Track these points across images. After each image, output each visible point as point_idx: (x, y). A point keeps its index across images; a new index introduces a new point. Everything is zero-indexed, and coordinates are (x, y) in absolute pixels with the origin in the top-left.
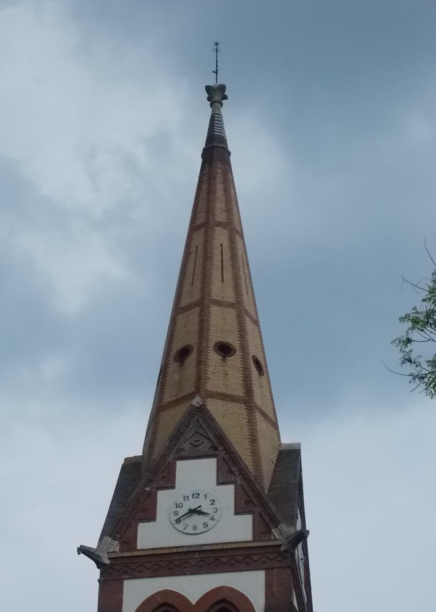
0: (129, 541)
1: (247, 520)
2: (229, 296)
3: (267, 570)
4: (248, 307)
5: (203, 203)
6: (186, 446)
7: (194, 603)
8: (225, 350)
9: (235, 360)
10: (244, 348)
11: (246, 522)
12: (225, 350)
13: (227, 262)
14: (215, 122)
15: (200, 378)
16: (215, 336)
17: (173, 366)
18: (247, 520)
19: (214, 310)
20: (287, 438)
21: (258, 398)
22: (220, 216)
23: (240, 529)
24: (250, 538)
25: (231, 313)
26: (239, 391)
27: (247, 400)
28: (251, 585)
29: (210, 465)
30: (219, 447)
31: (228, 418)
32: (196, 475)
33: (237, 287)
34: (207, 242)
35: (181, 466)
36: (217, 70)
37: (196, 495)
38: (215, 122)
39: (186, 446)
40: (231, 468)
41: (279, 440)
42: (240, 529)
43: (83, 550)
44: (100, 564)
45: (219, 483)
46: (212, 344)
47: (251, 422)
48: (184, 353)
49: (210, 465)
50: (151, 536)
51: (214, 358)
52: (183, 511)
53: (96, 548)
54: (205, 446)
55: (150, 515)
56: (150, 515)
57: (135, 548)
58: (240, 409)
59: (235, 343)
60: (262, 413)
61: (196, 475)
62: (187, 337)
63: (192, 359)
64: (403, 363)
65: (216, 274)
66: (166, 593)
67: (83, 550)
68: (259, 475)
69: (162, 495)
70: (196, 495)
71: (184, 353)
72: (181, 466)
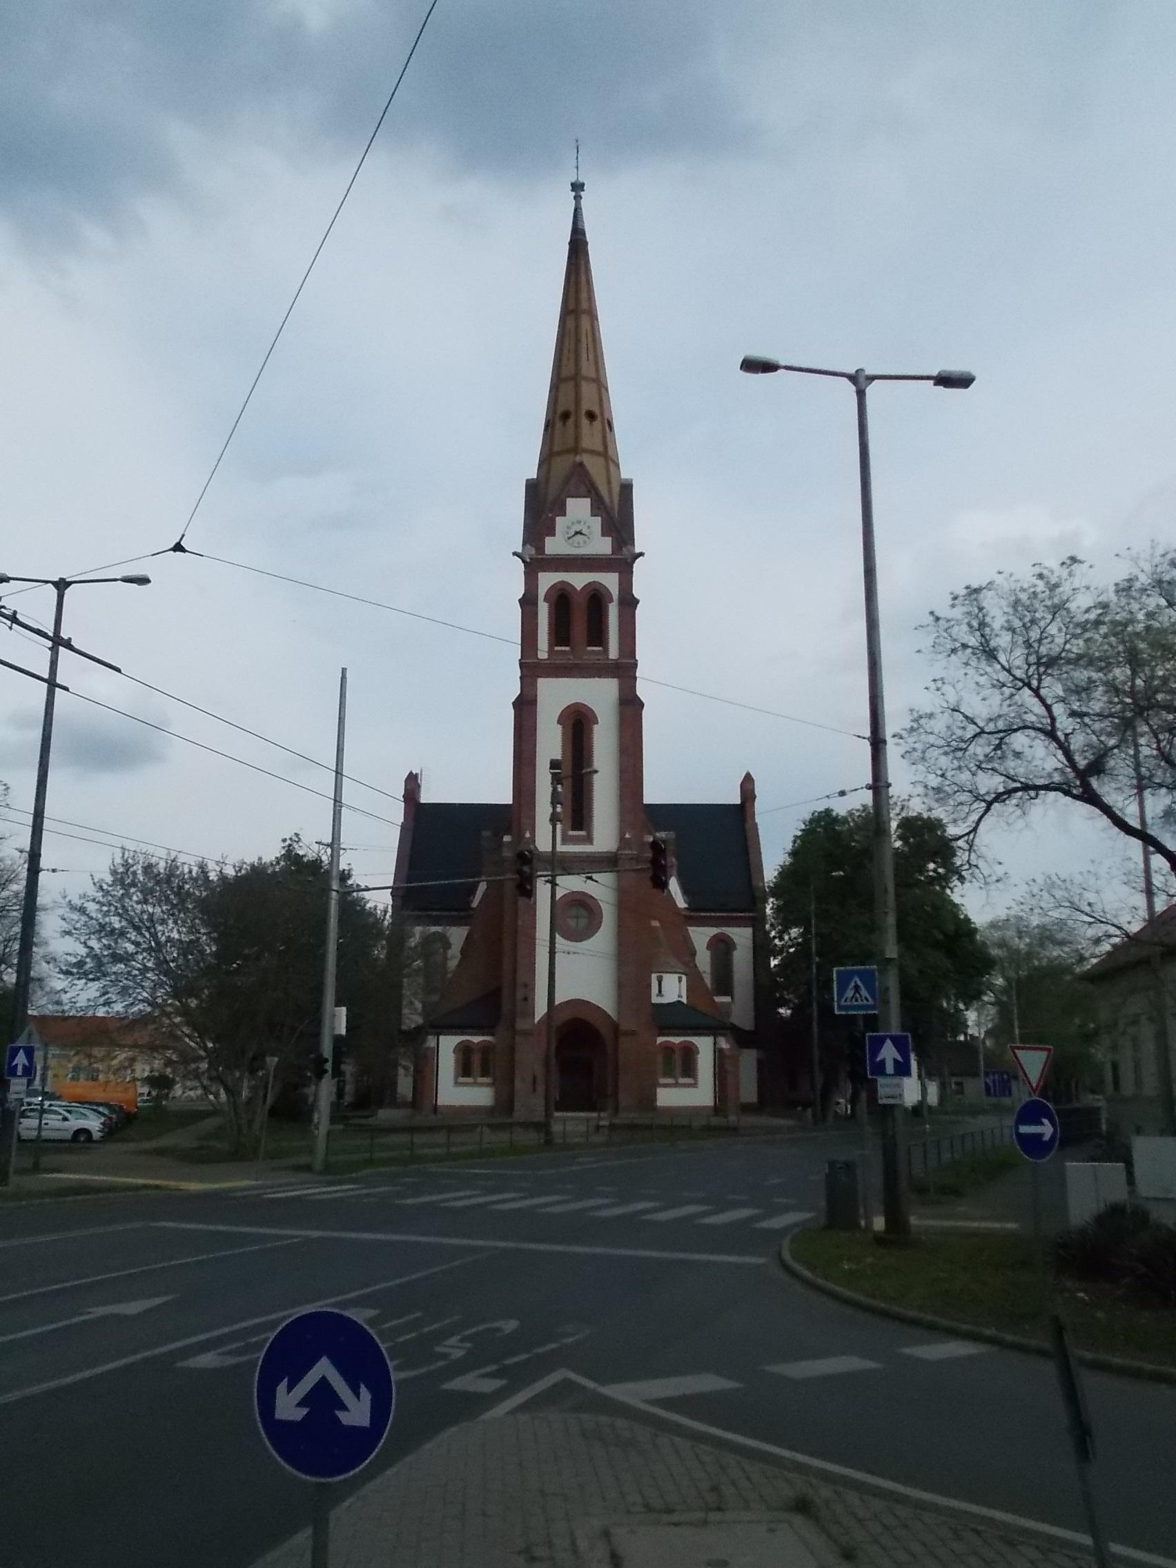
0: (540, 548)
2: (593, 375)
3: (620, 573)
8: (591, 416)
9: (597, 424)
10: (602, 414)
12: (591, 416)
13: (591, 349)
14: (577, 212)
15: (577, 438)
16: (586, 406)
17: (559, 424)
19: (584, 384)
20: (625, 475)
21: (610, 452)
22: (584, 305)
23: (602, 546)
24: (609, 552)
25: (594, 386)
26: (600, 448)
28: (610, 581)
29: (587, 502)
30: (591, 491)
31: (593, 465)
32: (578, 508)
33: (597, 370)
34: (577, 327)
37: (579, 522)
38: (577, 212)
40: (599, 507)
41: (754, 933)
42: (602, 546)
43: (515, 554)
44: (524, 561)
45: (603, 535)
48: (566, 416)
49: (587, 502)
50: (554, 546)
51: (585, 422)
54: (583, 489)
55: (552, 533)
56: (552, 533)
57: (543, 553)
59: (597, 412)
61: (578, 508)
62: (566, 404)
63: (571, 421)
65: (584, 356)
66: (563, 582)
67: (515, 554)
68: (613, 508)
70: (579, 522)
71: (566, 416)
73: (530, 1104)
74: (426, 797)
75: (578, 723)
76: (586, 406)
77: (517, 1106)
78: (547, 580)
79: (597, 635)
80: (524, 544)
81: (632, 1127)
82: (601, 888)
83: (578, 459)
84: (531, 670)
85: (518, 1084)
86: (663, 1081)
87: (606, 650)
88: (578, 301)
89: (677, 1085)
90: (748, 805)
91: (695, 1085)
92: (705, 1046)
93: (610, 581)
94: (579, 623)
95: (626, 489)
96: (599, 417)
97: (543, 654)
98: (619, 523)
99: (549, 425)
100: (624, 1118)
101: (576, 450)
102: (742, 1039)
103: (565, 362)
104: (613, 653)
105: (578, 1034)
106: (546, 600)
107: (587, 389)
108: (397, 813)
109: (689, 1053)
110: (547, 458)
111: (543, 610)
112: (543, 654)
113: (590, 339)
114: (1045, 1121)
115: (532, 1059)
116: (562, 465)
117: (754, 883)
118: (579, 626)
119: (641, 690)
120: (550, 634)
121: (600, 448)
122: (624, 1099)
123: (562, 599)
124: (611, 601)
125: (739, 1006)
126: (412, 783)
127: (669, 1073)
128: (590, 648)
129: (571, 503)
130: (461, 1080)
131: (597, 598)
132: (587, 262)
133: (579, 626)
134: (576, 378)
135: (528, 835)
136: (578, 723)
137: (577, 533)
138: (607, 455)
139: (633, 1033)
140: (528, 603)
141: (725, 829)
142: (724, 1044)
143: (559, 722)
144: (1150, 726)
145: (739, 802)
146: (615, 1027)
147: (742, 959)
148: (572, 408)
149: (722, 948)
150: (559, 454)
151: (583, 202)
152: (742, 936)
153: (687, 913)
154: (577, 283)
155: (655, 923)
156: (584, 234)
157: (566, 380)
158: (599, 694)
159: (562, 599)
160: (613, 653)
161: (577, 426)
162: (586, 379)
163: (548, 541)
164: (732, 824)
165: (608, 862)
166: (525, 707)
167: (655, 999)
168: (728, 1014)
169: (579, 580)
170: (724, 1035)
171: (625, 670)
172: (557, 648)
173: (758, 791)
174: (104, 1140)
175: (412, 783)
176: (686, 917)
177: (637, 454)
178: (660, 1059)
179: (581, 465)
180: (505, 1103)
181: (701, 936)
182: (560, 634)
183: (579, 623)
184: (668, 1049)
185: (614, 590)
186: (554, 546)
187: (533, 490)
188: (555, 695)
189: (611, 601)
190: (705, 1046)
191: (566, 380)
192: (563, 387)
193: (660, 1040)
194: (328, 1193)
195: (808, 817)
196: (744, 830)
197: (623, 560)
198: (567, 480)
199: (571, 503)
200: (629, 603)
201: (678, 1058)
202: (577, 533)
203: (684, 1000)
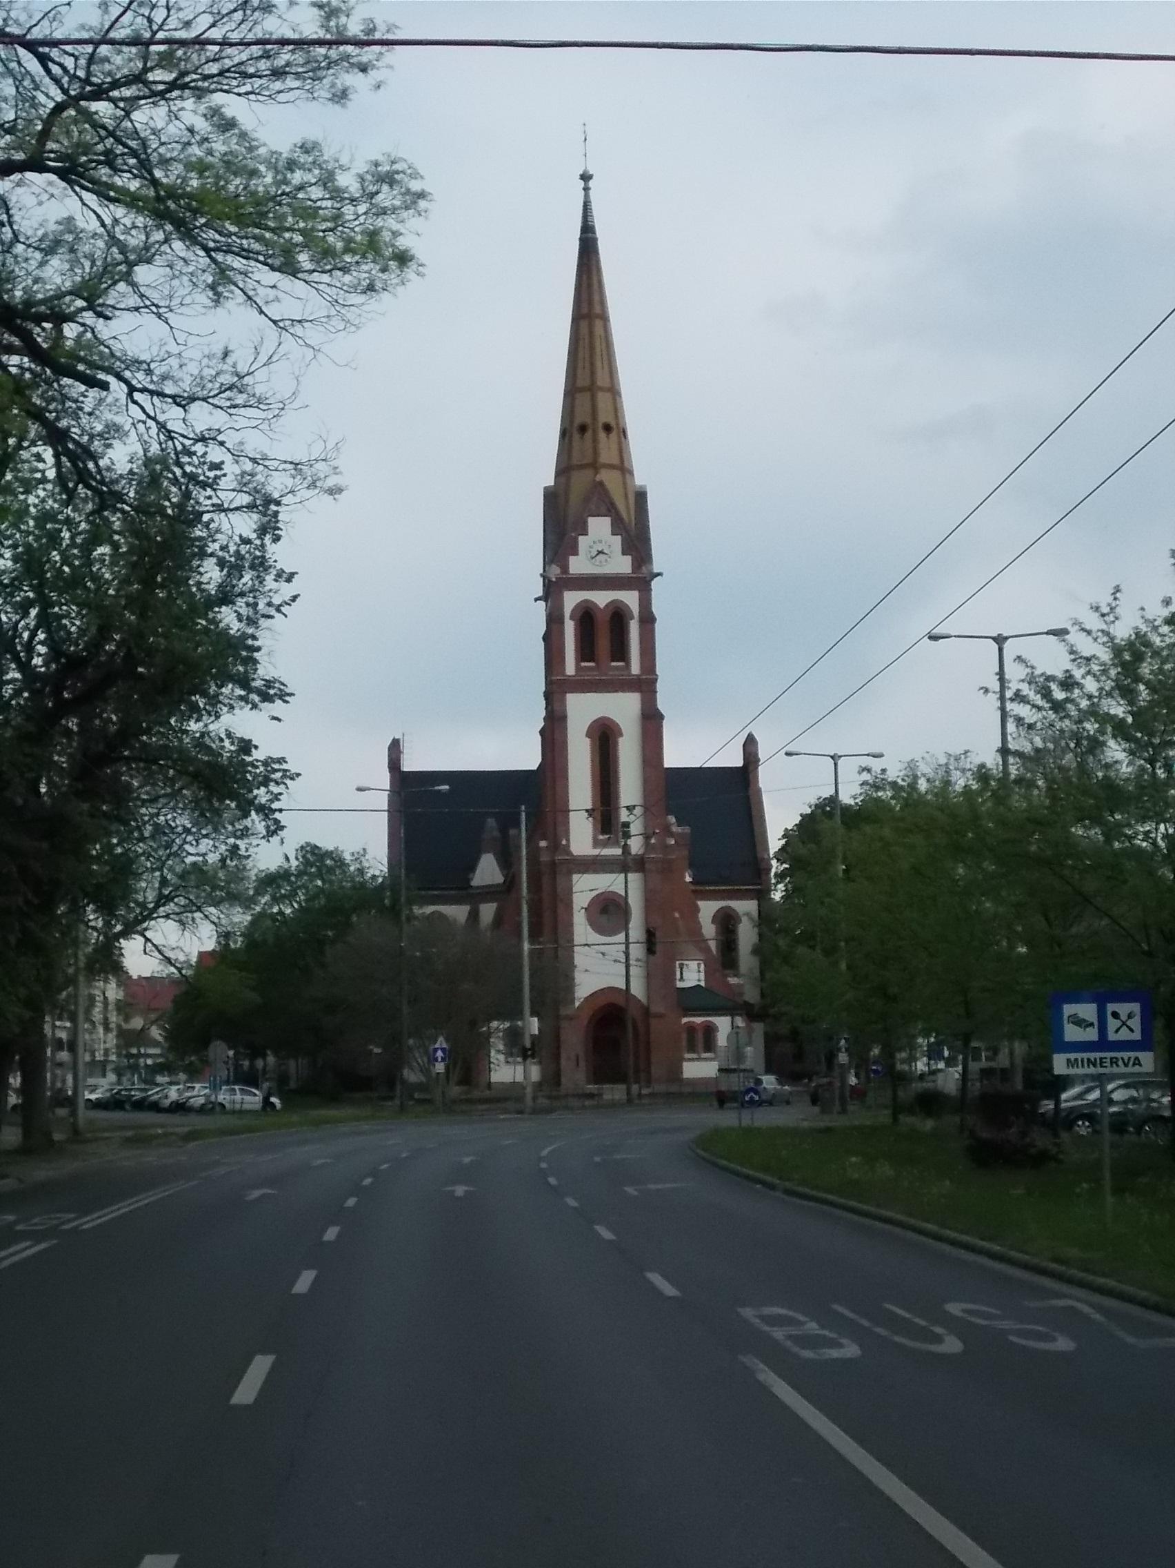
0: (565, 568)
1: (628, 559)
5: (584, 296)
6: (593, 507)
7: (699, 903)
8: (608, 428)
9: (613, 435)
10: (618, 424)
11: (628, 560)
13: (604, 353)
15: (596, 452)
16: (604, 417)
17: (576, 436)
18: (628, 559)
21: (626, 464)
22: (597, 309)
23: (622, 565)
25: (608, 395)
28: (631, 599)
29: (607, 521)
30: (610, 509)
31: (609, 478)
32: (599, 526)
34: (591, 333)
35: (591, 520)
36: (994, 639)
37: (600, 541)
39: (593, 507)
40: (618, 526)
42: (622, 565)
45: (624, 553)
46: (600, 425)
48: (583, 429)
49: (607, 521)
50: (578, 565)
51: (602, 435)
54: (603, 509)
56: (575, 552)
59: (613, 424)
61: (599, 526)
62: (582, 416)
63: (589, 434)
66: (586, 601)
69: (580, 538)
70: (600, 541)
71: (583, 429)
72: (591, 520)
73: (575, 1076)
75: (604, 737)
76: (604, 417)
77: (563, 1080)
78: (572, 599)
79: (620, 651)
81: (668, 1095)
82: (631, 887)
83: (598, 478)
85: (563, 1062)
86: (687, 1056)
88: (590, 303)
89: (699, 1059)
90: (751, 768)
93: (631, 599)
94: (600, 640)
96: (615, 429)
97: (570, 668)
98: (636, 541)
99: (564, 433)
100: (659, 1088)
101: (595, 466)
102: (752, 1013)
103: (579, 371)
104: (635, 668)
105: (611, 1014)
106: (571, 618)
107: (603, 400)
108: (383, 779)
109: (710, 1031)
110: (564, 470)
111: (570, 628)
112: (570, 668)
113: (604, 345)
115: (574, 1040)
116: (580, 481)
117: (759, 855)
118: (603, 643)
119: (661, 705)
120: (576, 651)
121: (616, 461)
122: (656, 1071)
123: (586, 616)
124: (632, 618)
125: (744, 980)
126: (395, 749)
127: (692, 1048)
128: (613, 664)
129: (592, 521)
131: (618, 616)
132: (598, 261)
133: (603, 643)
134: (592, 389)
135: (564, 842)
136: (604, 737)
137: (600, 552)
138: (624, 469)
139: (661, 1016)
141: (725, 797)
142: (740, 1022)
145: (740, 763)
146: (646, 1011)
147: (747, 935)
148: (588, 421)
149: (727, 922)
151: (591, 193)
152: (746, 907)
153: (693, 887)
154: (590, 286)
155: (677, 915)
156: (594, 232)
157: (581, 390)
158: (622, 708)
159: (586, 616)
160: (635, 668)
161: (595, 440)
162: (601, 389)
163: (572, 560)
164: (733, 790)
165: (640, 864)
167: (680, 985)
168: (741, 994)
169: (601, 598)
170: (740, 1015)
171: (646, 685)
172: (583, 664)
173: (762, 755)
174: (282, 1109)
175: (395, 749)
176: (694, 892)
178: (684, 1036)
179: (601, 484)
180: (552, 1079)
181: (708, 909)
182: (586, 650)
183: (600, 640)
184: (691, 1029)
185: (634, 607)
186: (578, 565)
187: (553, 499)
188: (583, 709)
189: (632, 618)
190: (723, 1024)
191: (581, 390)
193: (685, 1020)
194: (99, 1217)
195: (814, 801)
196: (748, 798)
197: (641, 580)
198: (587, 500)
199: (592, 521)
200: (648, 620)
201: (700, 1037)
202: (600, 552)
203: (703, 984)
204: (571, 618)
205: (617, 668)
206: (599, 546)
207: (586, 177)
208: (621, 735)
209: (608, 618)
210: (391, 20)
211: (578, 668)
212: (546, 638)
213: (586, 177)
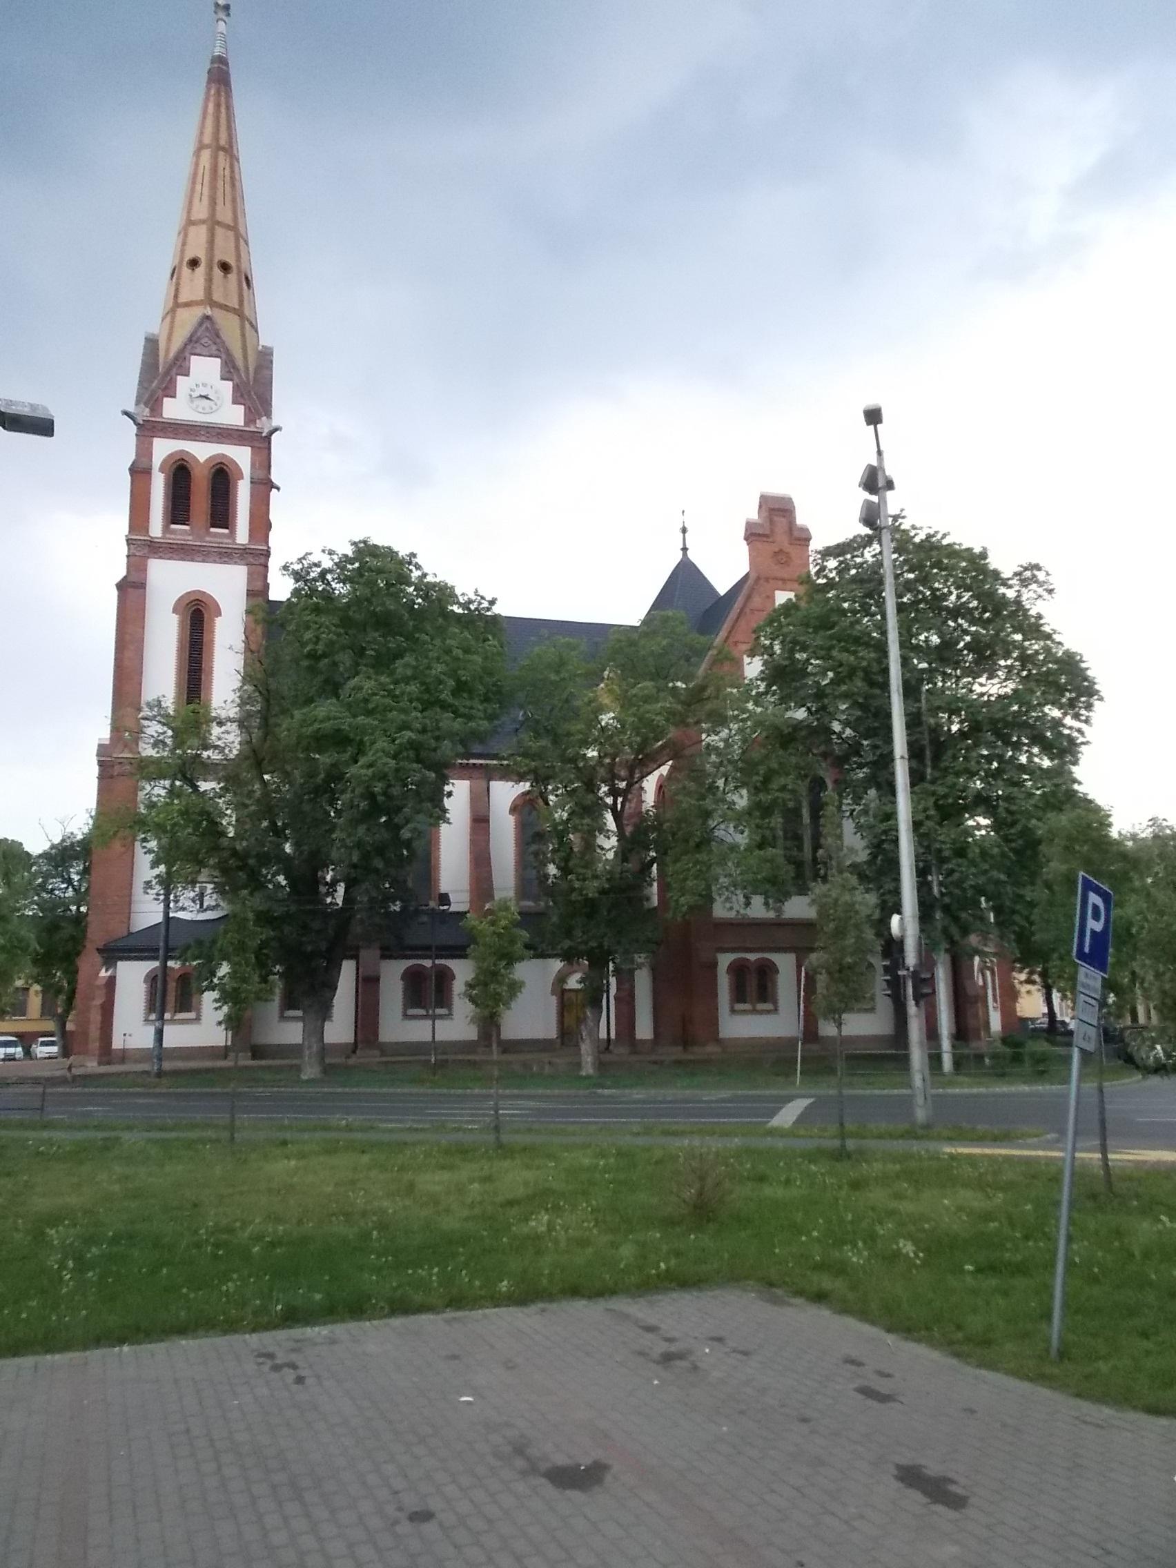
1: (240, 409)
4: (242, 230)
9: (233, 277)
10: (239, 268)
12: (225, 267)
16: (219, 256)
17: (186, 270)
18: (240, 409)
20: (265, 341)
23: (234, 416)
25: (219, 217)
27: (239, 313)
28: (241, 456)
29: (217, 362)
32: (205, 370)
37: (204, 385)
40: (229, 370)
42: (234, 416)
45: (234, 402)
47: (243, 328)
48: (194, 263)
49: (215, 364)
50: (173, 409)
51: (218, 272)
52: (195, 394)
53: (156, 440)
58: (235, 320)
59: (232, 262)
60: (251, 323)
61: (205, 370)
63: (201, 270)
64: (561, 658)
66: (183, 451)
67: (126, 413)
69: (179, 378)
70: (204, 385)
74: (274, 490)
75: (197, 615)
78: (163, 448)
79: (222, 515)
80: (137, 403)
84: (142, 548)
87: (233, 533)
91: (449, 1016)
92: (785, 963)
93: (241, 456)
95: (265, 359)
97: (156, 527)
98: (254, 388)
104: (242, 535)
106: (161, 470)
114: (579, 986)
120: (166, 495)
123: (180, 472)
128: (213, 530)
130: (411, 1012)
136: (197, 615)
140: (140, 473)
143: (175, 611)
144: (579, 675)
150: (188, 305)
159: (180, 472)
160: (242, 535)
166: (132, 590)
172: (173, 526)
177: (279, 319)
182: (178, 510)
186: (173, 409)
188: (171, 580)
192: (192, 229)
200: (264, 486)
204: (161, 470)
205: (216, 535)
206: (204, 392)
207: (684, 530)
208: (219, 614)
209: (206, 472)
210: (858, 474)
211: (166, 529)
212: (122, 586)
213: (684, 530)
